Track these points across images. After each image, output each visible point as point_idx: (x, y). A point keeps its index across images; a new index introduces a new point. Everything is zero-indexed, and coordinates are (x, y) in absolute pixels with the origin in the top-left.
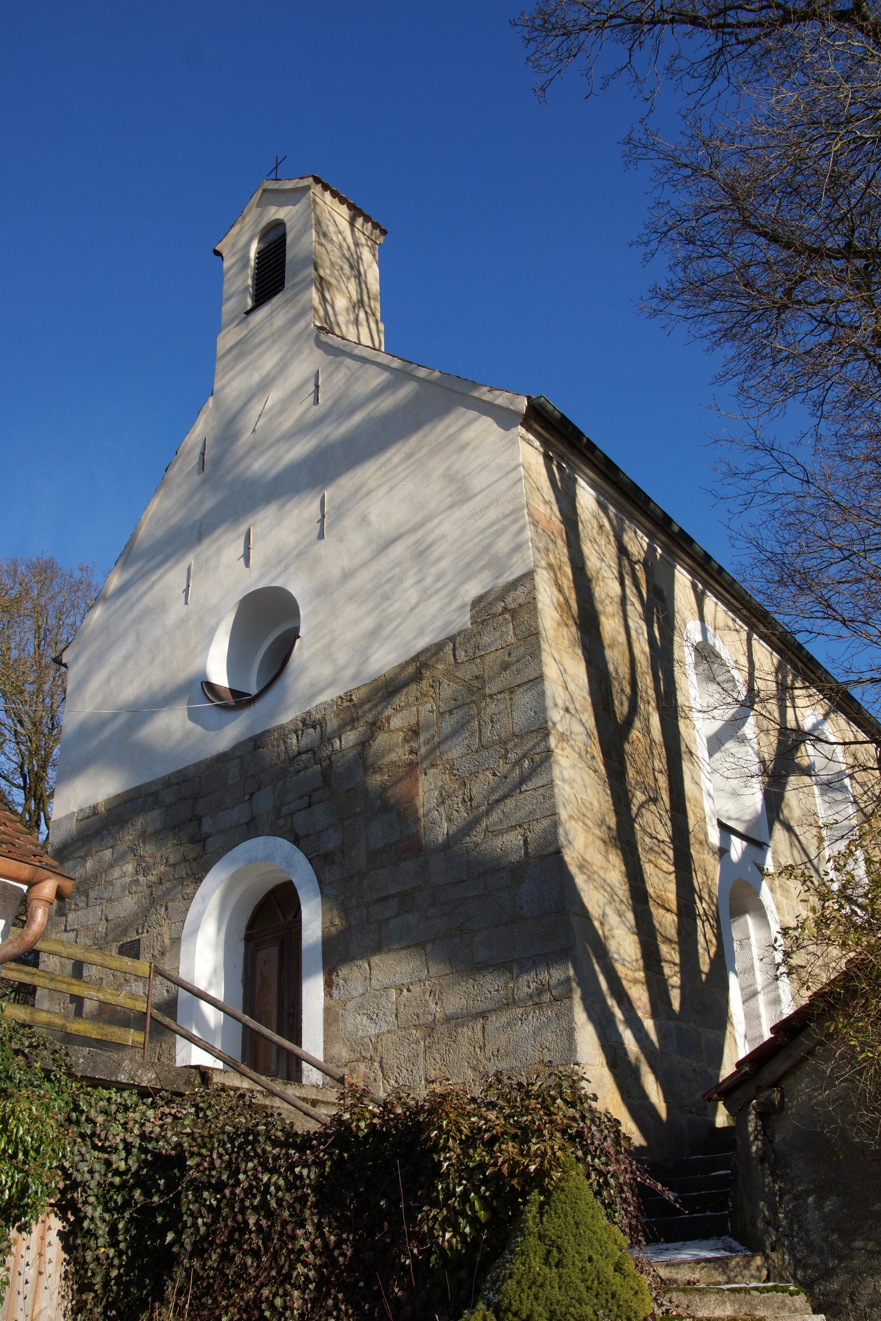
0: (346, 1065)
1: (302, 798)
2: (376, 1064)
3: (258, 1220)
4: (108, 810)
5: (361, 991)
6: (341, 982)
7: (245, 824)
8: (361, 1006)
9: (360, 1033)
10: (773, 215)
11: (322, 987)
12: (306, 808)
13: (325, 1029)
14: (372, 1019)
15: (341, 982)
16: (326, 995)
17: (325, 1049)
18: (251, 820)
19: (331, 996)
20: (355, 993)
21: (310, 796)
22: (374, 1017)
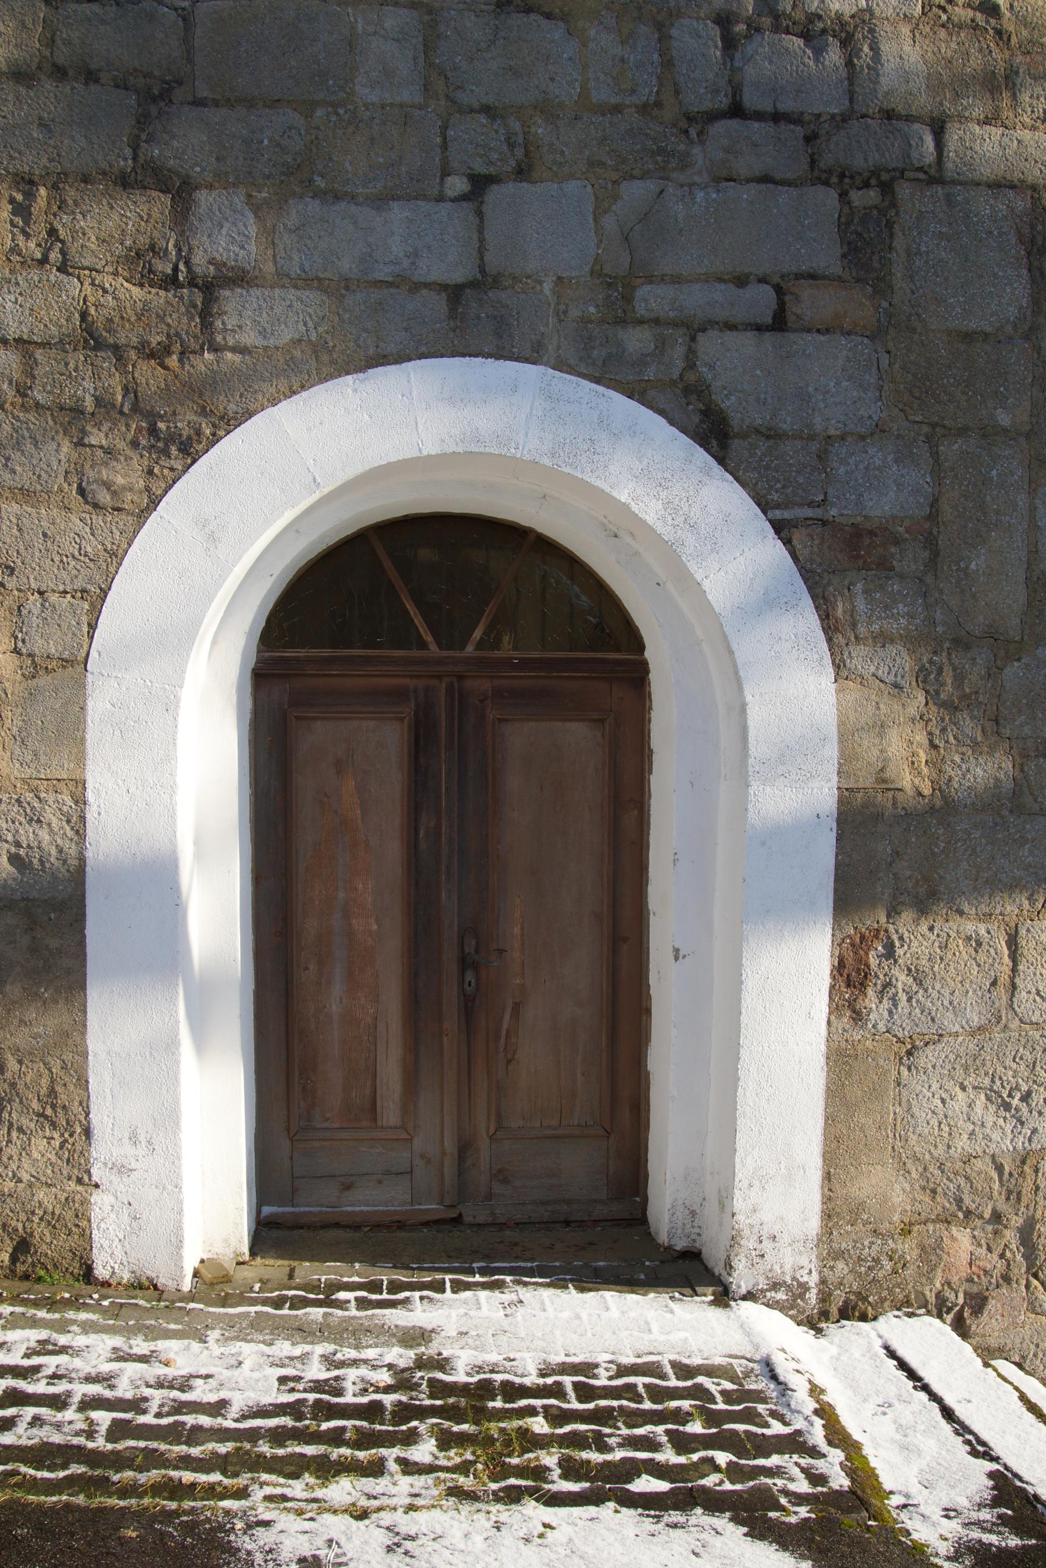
0: (906, 1232)
1: (741, 281)
2: (1011, 1236)
3: (717, 1469)
4: (722, 1511)
5: (976, 1021)
6: (902, 979)
7: (444, 287)
8: (973, 1063)
9: (962, 1144)
10: (908, 1208)
11: (825, 981)
12: (759, 328)
13: (830, 1120)
14: (1007, 1107)
15: (902, 979)
16: (835, 1009)
17: (828, 1177)
18: (473, 284)
19: (858, 1017)
20: (950, 1022)
21: (779, 290)
22: (1015, 1102)
